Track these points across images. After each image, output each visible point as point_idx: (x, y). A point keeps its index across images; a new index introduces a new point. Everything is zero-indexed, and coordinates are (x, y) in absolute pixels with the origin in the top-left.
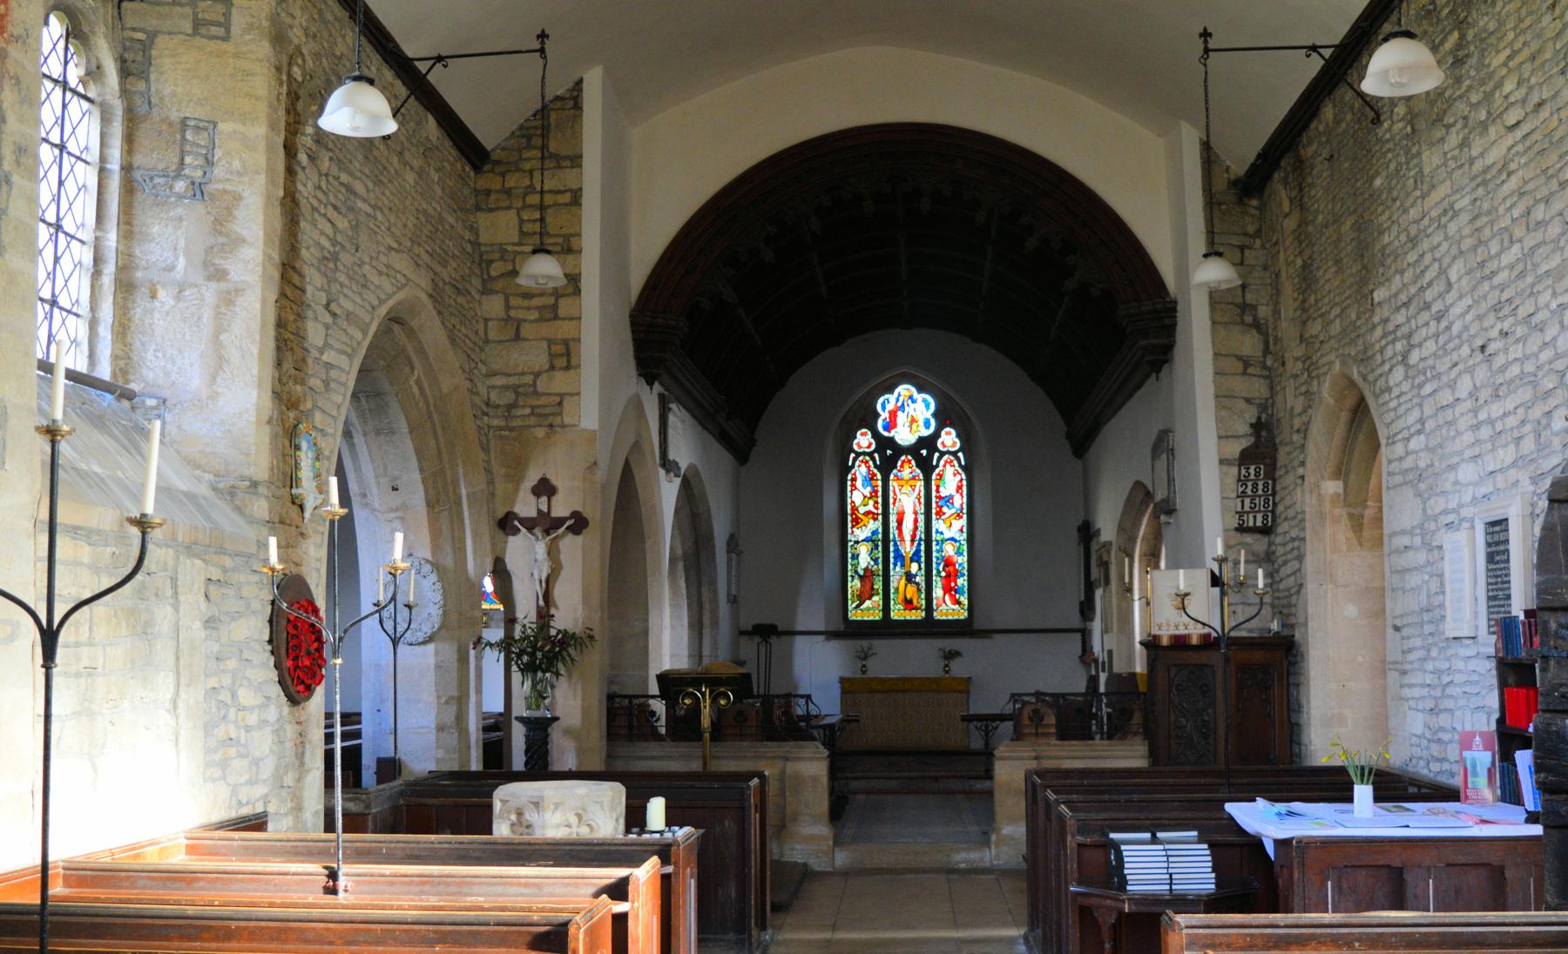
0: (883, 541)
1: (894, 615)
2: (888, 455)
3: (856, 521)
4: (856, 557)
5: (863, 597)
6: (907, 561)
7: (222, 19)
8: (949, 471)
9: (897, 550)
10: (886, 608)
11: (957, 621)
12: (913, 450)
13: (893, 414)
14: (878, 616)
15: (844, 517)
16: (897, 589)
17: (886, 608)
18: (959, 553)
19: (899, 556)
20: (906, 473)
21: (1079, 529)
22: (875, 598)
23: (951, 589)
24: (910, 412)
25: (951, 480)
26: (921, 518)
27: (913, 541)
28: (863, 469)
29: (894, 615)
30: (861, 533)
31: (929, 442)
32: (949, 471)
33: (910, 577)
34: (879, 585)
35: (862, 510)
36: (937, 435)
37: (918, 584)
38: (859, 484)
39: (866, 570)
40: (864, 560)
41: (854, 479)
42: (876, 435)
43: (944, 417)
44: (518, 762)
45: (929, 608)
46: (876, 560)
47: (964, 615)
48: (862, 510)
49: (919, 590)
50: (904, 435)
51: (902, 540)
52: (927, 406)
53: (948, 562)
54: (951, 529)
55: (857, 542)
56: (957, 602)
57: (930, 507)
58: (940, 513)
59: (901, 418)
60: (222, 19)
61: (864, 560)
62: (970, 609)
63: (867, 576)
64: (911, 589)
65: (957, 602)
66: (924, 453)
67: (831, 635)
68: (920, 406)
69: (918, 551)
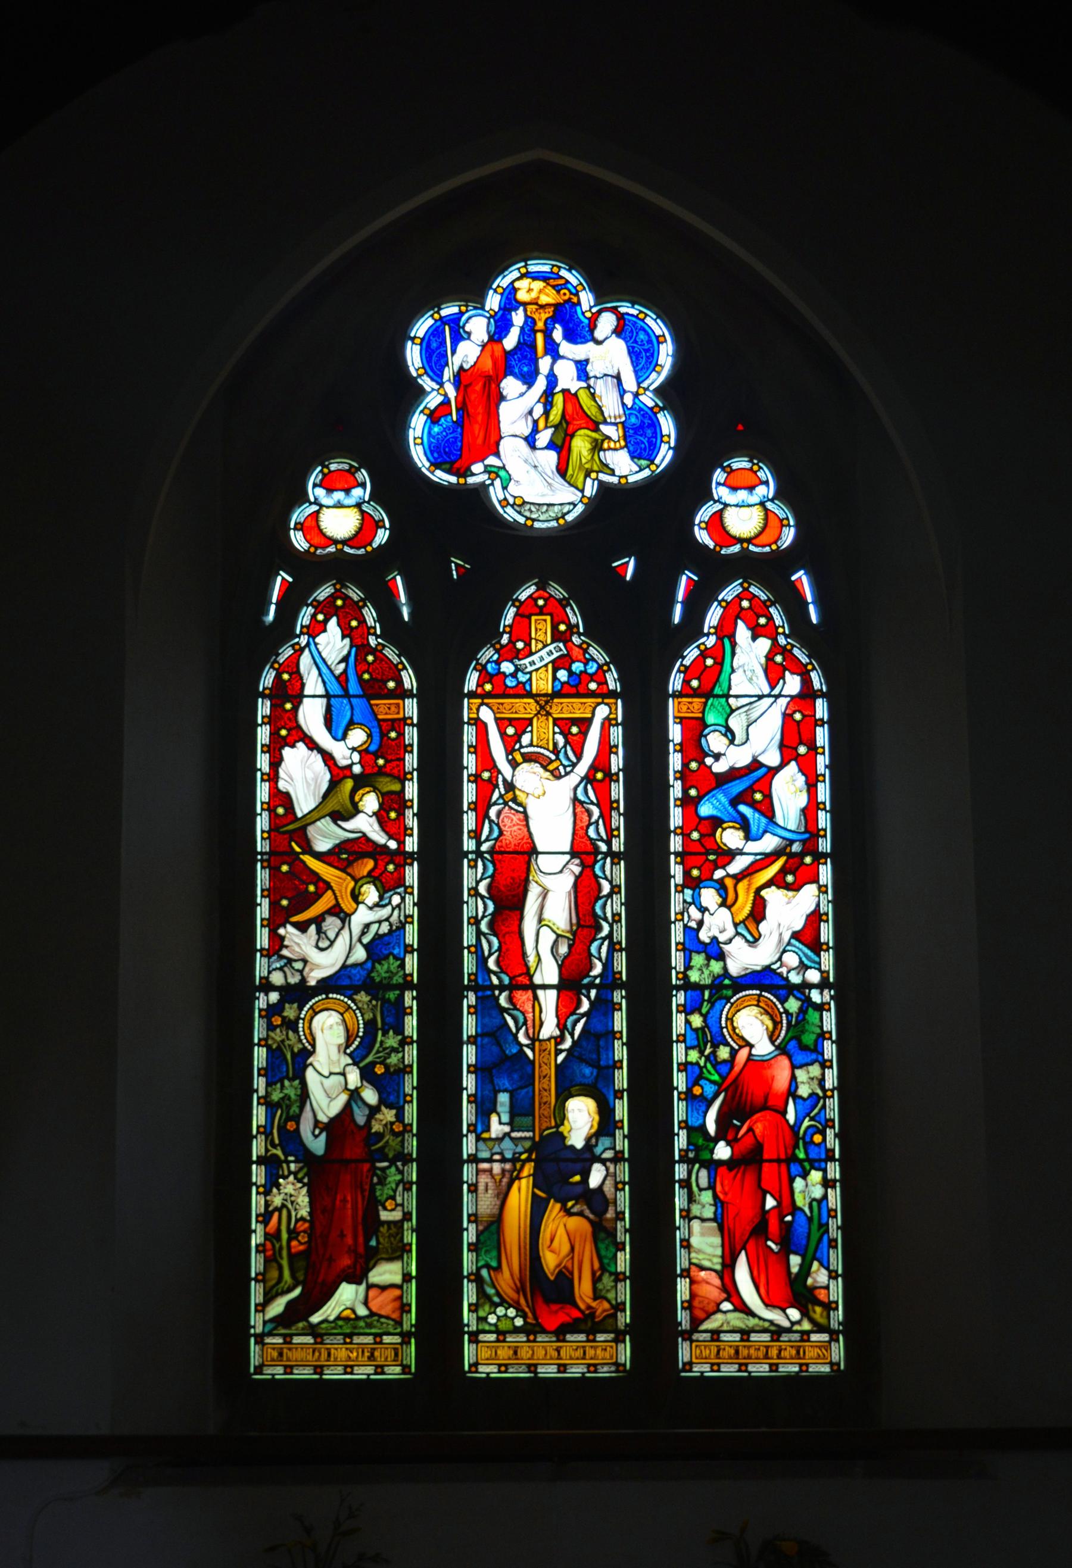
0: (433, 991)
1: (481, 1359)
2: (453, 570)
3: (297, 896)
4: (292, 1064)
5: (326, 1256)
6: (547, 1084)
7: (313, 929)
8: (750, 652)
9: (493, 1034)
10: (438, 1324)
11: (801, 1382)
12: (572, 555)
13: (480, 393)
14: (394, 1362)
15: (238, 865)
16: (492, 1228)
17: (438, 1324)
18: (795, 1043)
19: (505, 1064)
20: (539, 668)
21: (809, 917)
22: (386, 1273)
23: (760, 1228)
24: (556, 396)
25: (753, 706)
26: (613, 874)
27: (570, 984)
28: (333, 643)
29: (481, 1359)
30: (322, 955)
31: (644, 522)
32: (750, 652)
33: (557, 1169)
34: (399, 1207)
35: (325, 836)
36: (686, 485)
37: (596, 1200)
38: (311, 715)
39: (339, 1127)
40: (330, 1080)
41: (289, 692)
42: (395, 484)
43: (712, 415)
44: (498, 716)
45: (655, 1322)
46: (387, 1083)
47: (826, 1356)
48: (325, 836)
49: (602, 1232)
50: (530, 483)
51: (523, 981)
52: (642, 356)
53: (745, 1095)
54: (765, 928)
55: (299, 993)
56: (801, 1295)
57: (650, 835)
58: (706, 856)
59: (517, 404)
60: (313, 929)
61: (330, 1080)
62: (859, 1329)
63: (347, 1157)
64: (562, 1232)
65: (801, 1295)
66: (629, 574)
67: (144, 1457)
68: (610, 355)
69: (597, 1037)
